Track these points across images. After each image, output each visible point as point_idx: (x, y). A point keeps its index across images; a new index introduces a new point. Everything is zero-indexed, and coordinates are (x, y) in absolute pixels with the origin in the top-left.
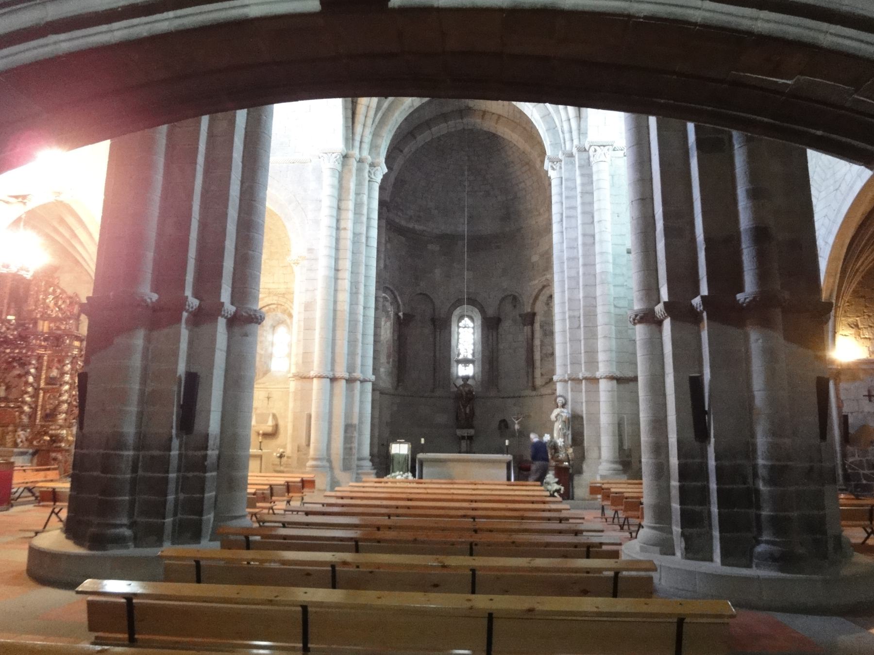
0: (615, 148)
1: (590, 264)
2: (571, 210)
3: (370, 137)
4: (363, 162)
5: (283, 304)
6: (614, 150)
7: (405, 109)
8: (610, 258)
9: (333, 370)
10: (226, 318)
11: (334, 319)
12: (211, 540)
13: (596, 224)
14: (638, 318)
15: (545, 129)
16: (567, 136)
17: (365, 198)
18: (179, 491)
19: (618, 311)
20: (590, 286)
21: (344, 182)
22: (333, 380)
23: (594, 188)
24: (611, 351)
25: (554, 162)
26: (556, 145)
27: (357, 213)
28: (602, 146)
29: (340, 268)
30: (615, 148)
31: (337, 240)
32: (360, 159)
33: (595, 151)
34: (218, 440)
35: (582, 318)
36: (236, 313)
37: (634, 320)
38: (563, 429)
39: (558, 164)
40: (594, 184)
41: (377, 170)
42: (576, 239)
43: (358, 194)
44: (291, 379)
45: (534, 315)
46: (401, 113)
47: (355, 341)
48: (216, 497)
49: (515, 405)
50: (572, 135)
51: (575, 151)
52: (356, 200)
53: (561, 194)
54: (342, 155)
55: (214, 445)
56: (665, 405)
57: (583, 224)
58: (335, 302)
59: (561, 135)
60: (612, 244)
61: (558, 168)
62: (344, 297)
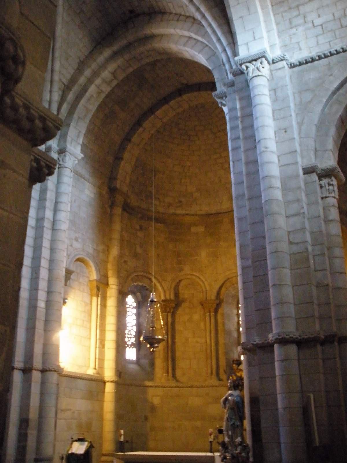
19: (295, 249)
25: (223, 98)
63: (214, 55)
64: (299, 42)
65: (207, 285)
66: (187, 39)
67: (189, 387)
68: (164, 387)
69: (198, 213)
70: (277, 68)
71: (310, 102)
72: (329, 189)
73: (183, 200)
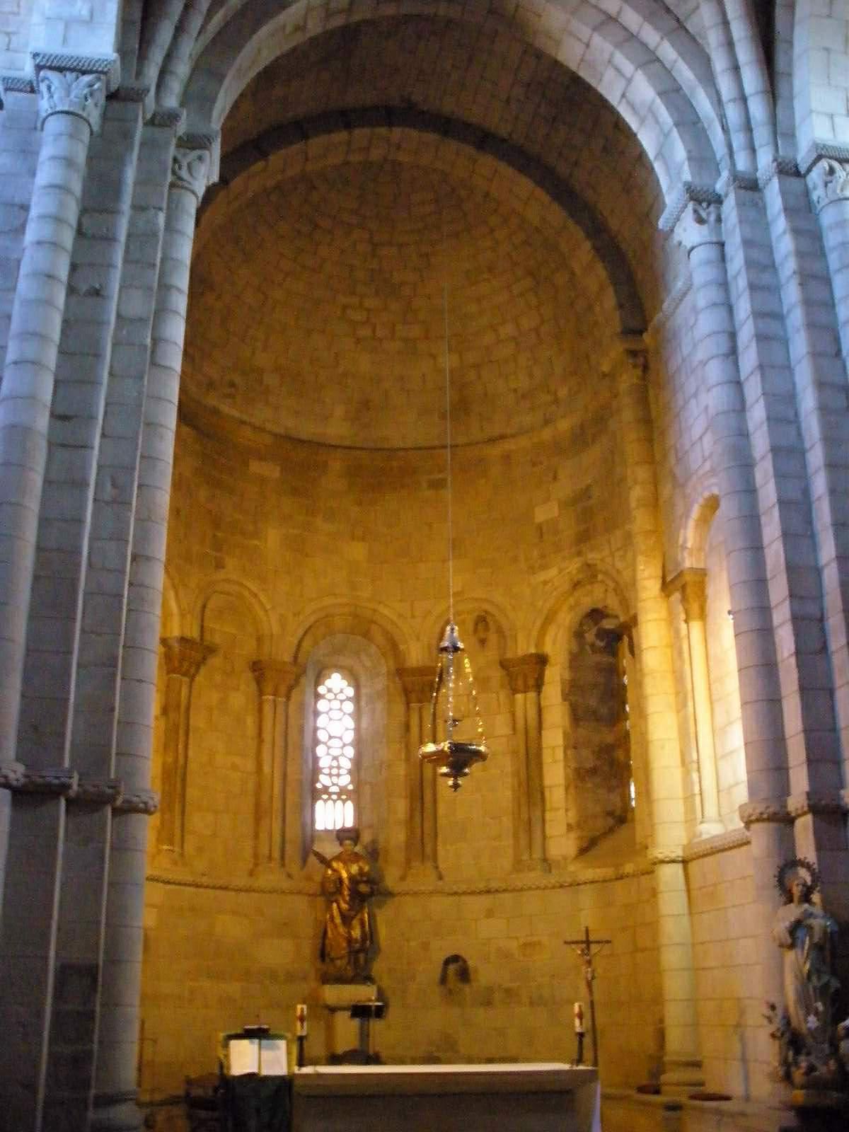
7: (284, 27)
16: (738, 140)
33: (832, 171)
38: (819, 972)
39: (712, 208)
45: (541, 661)
49: (490, 914)
61: (712, 218)
66: (603, 17)
67: (221, 888)
68: (169, 883)
73: (238, 380)
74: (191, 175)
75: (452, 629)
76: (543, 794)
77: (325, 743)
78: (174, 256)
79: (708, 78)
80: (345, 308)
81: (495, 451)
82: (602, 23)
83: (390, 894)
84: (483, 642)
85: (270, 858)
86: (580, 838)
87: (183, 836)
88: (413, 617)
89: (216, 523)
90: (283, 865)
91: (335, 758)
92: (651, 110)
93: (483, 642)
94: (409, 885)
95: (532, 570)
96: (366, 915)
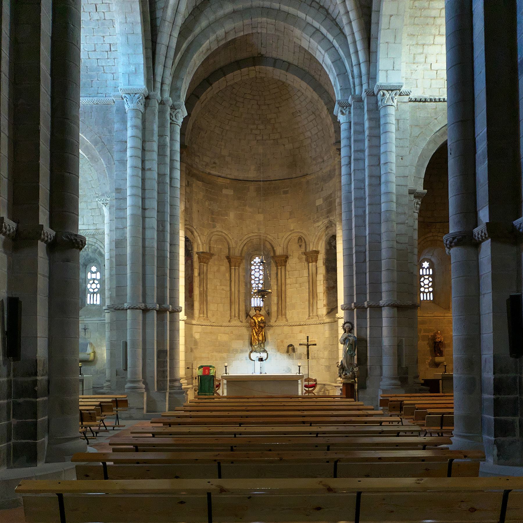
0: (401, 92)
1: (376, 203)
2: (359, 153)
3: (170, 79)
4: (164, 104)
5: (94, 244)
6: (400, 95)
8: (394, 198)
9: (144, 301)
10: (46, 242)
11: (144, 255)
12: (46, 462)
13: (382, 166)
14: (456, 240)
15: (336, 74)
16: (357, 81)
17: (168, 139)
18: (11, 417)
20: (376, 223)
21: (147, 124)
22: (145, 311)
23: (381, 132)
24: (393, 282)
26: (346, 89)
27: (161, 154)
28: (390, 90)
29: (147, 207)
30: (401, 92)
31: (143, 180)
32: (162, 100)
33: (384, 95)
34: (47, 365)
35: (367, 253)
36: (56, 237)
37: (451, 242)
40: (381, 128)
41: (178, 112)
42: (363, 181)
43: (161, 136)
44: (106, 311)
45: (317, 252)
46: (199, 55)
47: (164, 276)
48: (49, 421)
49: (301, 332)
50: (361, 79)
51: (364, 95)
52: (159, 142)
53: (349, 138)
54: (144, 95)
55: (43, 370)
56: (478, 324)
57: (370, 166)
58: (144, 239)
59: (351, 80)
60: (396, 185)
61: (347, 113)
62: (152, 234)
63: (339, 60)
64: (417, 79)
65: (233, 243)
69: (229, 176)
70: (403, 101)
71: (417, 137)
72: (416, 207)
73: (217, 161)
74: (176, 118)
75: (262, 257)
76: (317, 295)
77: (254, 280)
78: (173, 149)
79: (349, 56)
80: (252, 130)
81: (304, 180)
82: (314, 33)
83: (272, 326)
84: (300, 246)
85: (235, 316)
86: (328, 309)
87: (207, 311)
88: (278, 238)
89: (212, 213)
90: (239, 319)
91: (257, 284)
92: (331, 68)
93: (300, 246)
94: (276, 324)
95: (315, 222)
96: (263, 333)
